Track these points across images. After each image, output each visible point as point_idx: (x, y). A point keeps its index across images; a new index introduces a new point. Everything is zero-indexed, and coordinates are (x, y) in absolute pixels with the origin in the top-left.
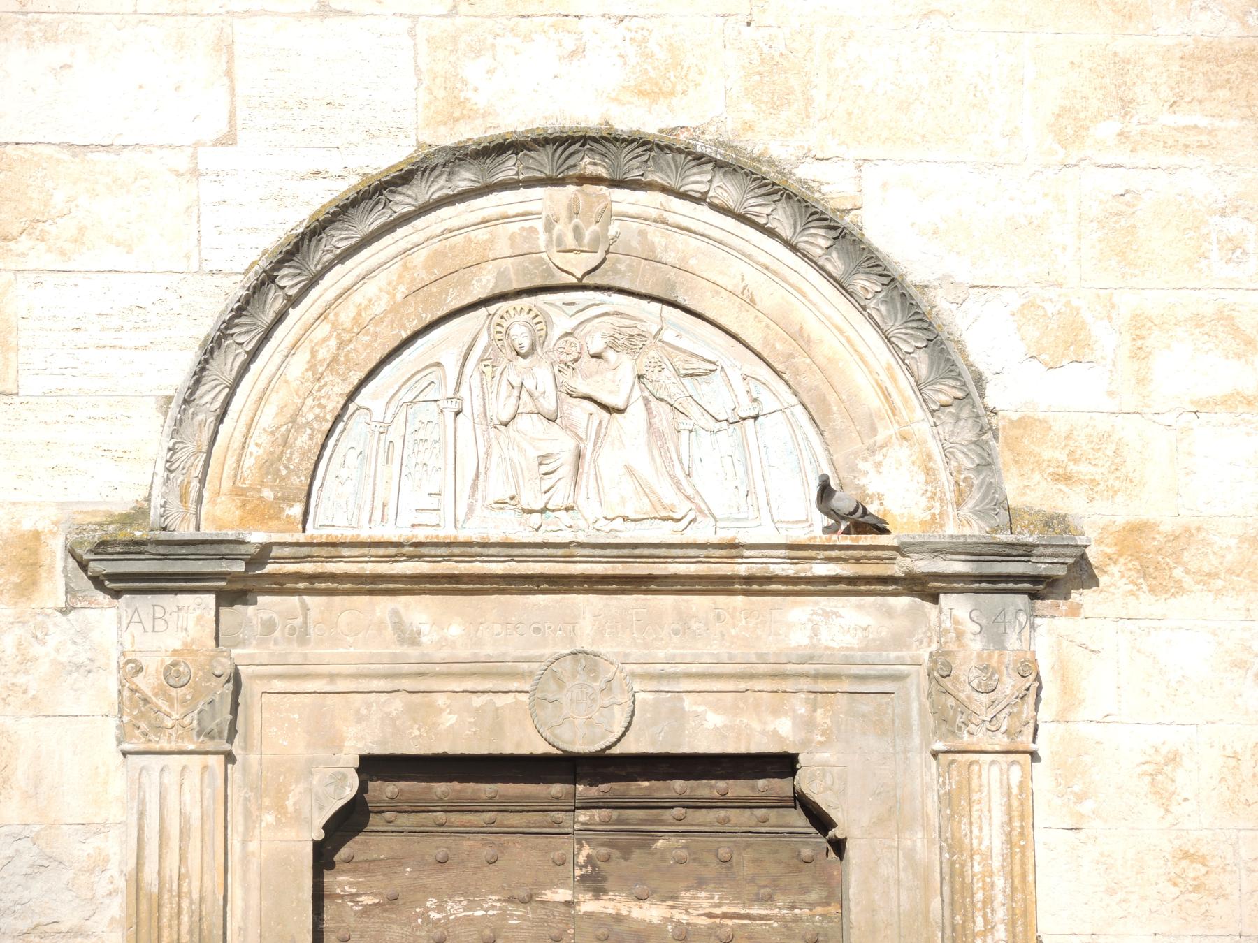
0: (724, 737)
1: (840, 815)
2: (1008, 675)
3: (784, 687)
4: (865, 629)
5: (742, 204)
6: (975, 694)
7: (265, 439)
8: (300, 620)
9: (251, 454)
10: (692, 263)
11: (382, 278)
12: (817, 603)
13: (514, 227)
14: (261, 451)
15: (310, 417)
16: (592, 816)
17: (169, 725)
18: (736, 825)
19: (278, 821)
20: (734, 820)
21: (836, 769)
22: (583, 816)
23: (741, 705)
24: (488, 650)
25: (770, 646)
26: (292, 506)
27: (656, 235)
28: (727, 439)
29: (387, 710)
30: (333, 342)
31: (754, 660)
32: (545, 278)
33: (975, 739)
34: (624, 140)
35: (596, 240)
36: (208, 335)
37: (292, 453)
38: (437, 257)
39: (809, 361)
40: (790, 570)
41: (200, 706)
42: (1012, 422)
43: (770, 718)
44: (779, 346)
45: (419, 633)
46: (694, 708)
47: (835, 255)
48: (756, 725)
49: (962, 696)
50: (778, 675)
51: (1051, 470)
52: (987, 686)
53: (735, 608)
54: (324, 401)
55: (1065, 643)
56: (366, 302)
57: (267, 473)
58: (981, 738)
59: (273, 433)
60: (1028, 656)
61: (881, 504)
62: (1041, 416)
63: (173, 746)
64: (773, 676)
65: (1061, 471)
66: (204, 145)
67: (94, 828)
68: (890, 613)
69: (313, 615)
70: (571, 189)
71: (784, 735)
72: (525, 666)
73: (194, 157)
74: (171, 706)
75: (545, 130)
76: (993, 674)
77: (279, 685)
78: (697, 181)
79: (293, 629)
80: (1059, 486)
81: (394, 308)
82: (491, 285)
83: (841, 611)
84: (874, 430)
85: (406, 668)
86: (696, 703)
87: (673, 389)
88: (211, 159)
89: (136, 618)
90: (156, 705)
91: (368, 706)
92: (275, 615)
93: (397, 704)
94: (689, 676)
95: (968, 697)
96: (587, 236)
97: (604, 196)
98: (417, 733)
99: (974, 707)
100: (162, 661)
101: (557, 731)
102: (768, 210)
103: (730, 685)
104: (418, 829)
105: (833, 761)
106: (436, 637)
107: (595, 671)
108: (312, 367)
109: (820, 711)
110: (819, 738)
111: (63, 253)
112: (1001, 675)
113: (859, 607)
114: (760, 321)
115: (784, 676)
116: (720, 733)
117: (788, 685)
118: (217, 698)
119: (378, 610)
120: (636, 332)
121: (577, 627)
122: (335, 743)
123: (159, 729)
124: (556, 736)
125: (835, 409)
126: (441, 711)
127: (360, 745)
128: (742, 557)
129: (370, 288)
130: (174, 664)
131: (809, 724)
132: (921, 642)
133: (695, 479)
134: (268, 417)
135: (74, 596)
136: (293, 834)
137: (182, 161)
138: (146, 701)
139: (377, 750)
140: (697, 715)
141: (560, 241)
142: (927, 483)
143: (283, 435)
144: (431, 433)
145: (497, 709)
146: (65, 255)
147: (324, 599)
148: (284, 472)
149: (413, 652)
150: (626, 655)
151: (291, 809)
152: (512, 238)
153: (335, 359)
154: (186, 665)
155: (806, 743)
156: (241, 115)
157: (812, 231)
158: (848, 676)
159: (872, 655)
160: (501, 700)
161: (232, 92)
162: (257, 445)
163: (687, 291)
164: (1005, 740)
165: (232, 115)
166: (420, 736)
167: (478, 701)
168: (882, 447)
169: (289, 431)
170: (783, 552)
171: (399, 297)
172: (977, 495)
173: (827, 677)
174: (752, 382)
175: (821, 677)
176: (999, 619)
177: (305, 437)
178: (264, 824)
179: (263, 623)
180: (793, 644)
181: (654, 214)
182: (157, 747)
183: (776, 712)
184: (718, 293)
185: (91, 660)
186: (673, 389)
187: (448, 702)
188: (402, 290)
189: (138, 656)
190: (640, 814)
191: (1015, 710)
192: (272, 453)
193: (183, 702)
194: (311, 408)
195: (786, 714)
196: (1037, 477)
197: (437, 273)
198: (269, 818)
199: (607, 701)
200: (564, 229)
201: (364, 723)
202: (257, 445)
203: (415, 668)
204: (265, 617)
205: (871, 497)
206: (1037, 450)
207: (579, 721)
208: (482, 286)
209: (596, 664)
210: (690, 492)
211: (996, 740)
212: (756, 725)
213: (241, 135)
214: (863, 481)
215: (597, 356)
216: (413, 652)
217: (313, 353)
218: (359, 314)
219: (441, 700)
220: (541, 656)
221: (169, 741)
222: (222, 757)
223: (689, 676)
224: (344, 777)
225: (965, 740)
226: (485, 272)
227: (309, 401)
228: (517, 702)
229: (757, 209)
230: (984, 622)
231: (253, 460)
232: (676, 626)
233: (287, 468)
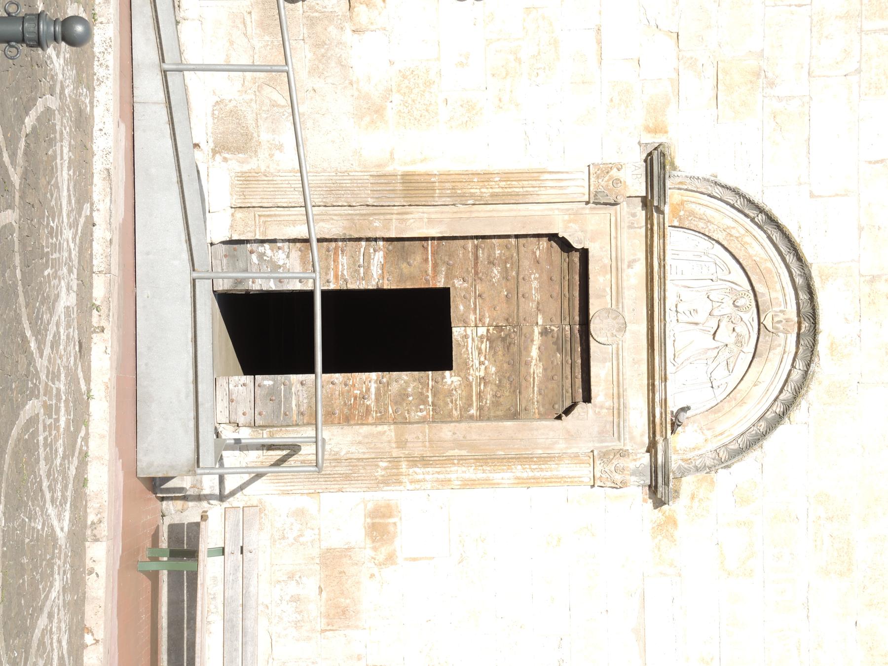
10: (768, 364)
15: (710, 227)
22: (568, 328)
27: (780, 350)
30: (737, 235)
35: (777, 328)
58: (598, 467)
63: (592, 183)
68: (642, 435)
70: (796, 319)
78: (800, 365)
81: (750, 256)
85: (619, 264)
93: (607, 261)
94: (618, 364)
96: (779, 325)
108: (728, 228)
115: (619, 398)
117: (616, 400)
122: (592, 240)
123: (598, 177)
131: (601, 407)
134: (709, 213)
139: (590, 255)
141: (776, 315)
149: (625, 266)
155: (595, 406)
159: (627, 429)
160: (608, 298)
171: (754, 258)
173: (619, 413)
175: (619, 411)
181: (787, 349)
183: (606, 395)
188: (757, 259)
197: (764, 272)
198: (566, 217)
200: (781, 317)
208: (759, 288)
215: (734, 330)
216: (625, 266)
217: (733, 228)
219: (608, 276)
225: (598, 462)
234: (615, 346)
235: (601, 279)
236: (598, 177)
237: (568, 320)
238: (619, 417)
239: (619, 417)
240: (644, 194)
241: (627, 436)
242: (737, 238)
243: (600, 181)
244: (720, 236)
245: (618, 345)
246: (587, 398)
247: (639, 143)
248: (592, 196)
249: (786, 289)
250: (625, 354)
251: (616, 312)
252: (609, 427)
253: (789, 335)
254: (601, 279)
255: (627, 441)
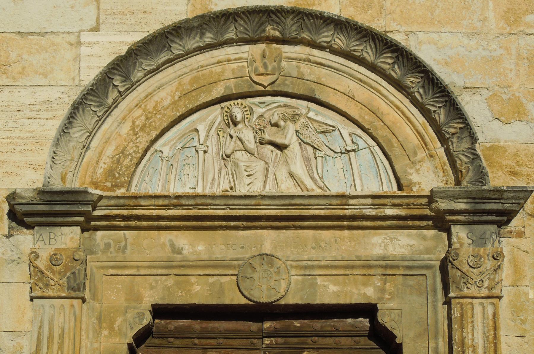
0: (338, 296)
1: (398, 332)
2: (489, 259)
3: (370, 273)
4: (411, 246)
5: (348, 45)
6: (471, 269)
7: (108, 161)
8: (123, 243)
9: (101, 167)
10: (323, 80)
11: (168, 89)
12: (386, 234)
13: (234, 66)
14: (106, 166)
15: (131, 151)
16: (271, 341)
17: (53, 284)
18: (344, 345)
19: (110, 334)
20: (343, 342)
21: (396, 311)
22: (267, 341)
23: (347, 281)
24: (218, 255)
25: (362, 253)
26: (120, 189)
27: (305, 69)
28: (340, 162)
29: (165, 283)
30: (143, 118)
31: (355, 259)
32: (250, 88)
33: (470, 291)
34: (288, 11)
35: (274, 69)
36: (76, 100)
37: (121, 167)
38: (195, 79)
39: (382, 124)
40: (373, 212)
41: (68, 275)
42: (487, 148)
43: (362, 288)
44: (366, 117)
45: (182, 249)
46: (323, 283)
47: (396, 66)
48: (355, 291)
49: (464, 270)
50: (367, 266)
51: (506, 170)
52: (478, 264)
53: (344, 237)
54: (138, 144)
55: (516, 249)
56: (160, 100)
57: (109, 176)
58: (473, 291)
59: (112, 158)
60: (499, 250)
61: (420, 187)
62: (502, 145)
63: (55, 294)
64: (363, 267)
65: (512, 170)
66: (84, 31)
67: (17, 334)
68: (424, 238)
69: (130, 241)
70: (262, 46)
71: (369, 295)
72: (236, 262)
73: (79, 36)
74: (54, 275)
75: (248, 7)
76: (480, 258)
77: (112, 271)
78: (326, 36)
79: (120, 247)
80: (512, 177)
81: (174, 103)
82: (222, 92)
83: (399, 238)
84: (415, 154)
85: (175, 263)
86: (324, 281)
87: (314, 138)
88: (86, 37)
89: (41, 238)
90: (46, 274)
91: (156, 282)
92: (111, 241)
93: (170, 281)
94: (320, 267)
95: (467, 271)
96: (270, 68)
97: (279, 49)
98: (180, 294)
99: (470, 275)
100: (50, 253)
101: (252, 292)
102: (361, 48)
103: (342, 272)
104: (184, 346)
105: (395, 307)
106: (191, 250)
107: (271, 264)
108: (133, 129)
109: (388, 284)
110: (387, 296)
111: (14, 78)
112: (485, 260)
113: (408, 236)
114: (357, 106)
115: (370, 267)
116: (336, 294)
117: (372, 272)
118: (77, 272)
119: (162, 238)
120: (295, 113)
121: (263, 246)
122: (139, 299)
123: (47, 285)
124: (251, 295)
125: (395, 145)
126: (193, 284)
127: (151, 300)
128: (349, 205)
129: (162, 94)
130: (55, 254)
131: (383, 290)
132: (440, 252)
133: (325, 179)
134: (110, 151)
135: (13, 230)
136: (118, 340)
137: (72, 39)
138: (42, 273)
139: (160, 302)
140: (325, 286)
141: (256, 69)
142: (443, 176)
143: (117, 159)
144: (191, 161)
145: (221, 283)
146: (15, 79)
147: (135, 232)
148: (117, 175)
149: (179, 257)
150: (288, 257)
151: (117, 329)
152: (233, 70)
153: (144, 126)
154: (61, 255)
155: (381, 299)
156: (102, 17)
157: (385, 55)
158: (403, 267)
159: (416, 257)
160: (223, 279)
161: (98, 8)
162: (105, 163)
163: (320, 93)
164: (487, 291)
165: (98, 19)
166: (182, 296)
167: (211, 280)
168: (420, 162)
169: (120, 157)
170: (369, 201)
171: (176, 98)
172: (470, 174)
173: (392, 267)
174: (353, 136)
175: (387, 267)
176: (482, 237)
177: (128, 160)
178: (103, 335)
179: (106, 244)
180: (375, 253)
181: (304, 56)
182: (47, 295)
183: (365, 284)
184: (336, 94)
185: (19, 258)
186: (314, 138)
187: (196, 280)
188: (178, 94)
189: (37, 251)
190: (295, 340)
191: (492, 277)
192: (112, 167)
193: (60, 273)
194: (132, 148)
195: (371, 286)
196: (500, 173)
197: (195, 86)
198: (105, 333)
199: (277, 278)
200: (259, 64)
201: (154, 290)
202: (105, 163)
203: (180, 263)
204: (106, 241)
205: (415, 183)
206: (500, 160)
207: (264, 288)
208: (218, 91)
209: (272, 260)
210: (322, 185)
211: (482, 292)
212: (355, 291)
213: (102, 27)
214: (411, 177)
215: (276, 125)
216: (179, 257)
217: (134, 122)
218: (156, 105)
219: (193, 279)
220: (244, 258)
221: (53, 292)
222: (81, 300)
223: (320, 267)
224: (144, 314)
225: (466, 292)
226: (219, 86)
227: (131, 144)
228: (232, 280)
229: (356, 48)
230: (474, 238)
231: (102, 170)
232: (314, 245)
233: (119, 173)
234: (293, 272)
235: (197, 288)
236: (47, 285)
237: (255, 341)
238: (397, 267)
239: (397, 267)
240: (78, 229)
241: (426, 257)
242: (147, 118)
243: (52, 283)
244: (144, 141)
245: (292, 266)
246: (369, 310)
247: (8, 236)
248: (73, 294)
249: (222, 58)
250: (306, 257)
251: (242, 270)
252: (411, 281)
253: (284, 55)
254: (197, 288)
255: (432, 256)
